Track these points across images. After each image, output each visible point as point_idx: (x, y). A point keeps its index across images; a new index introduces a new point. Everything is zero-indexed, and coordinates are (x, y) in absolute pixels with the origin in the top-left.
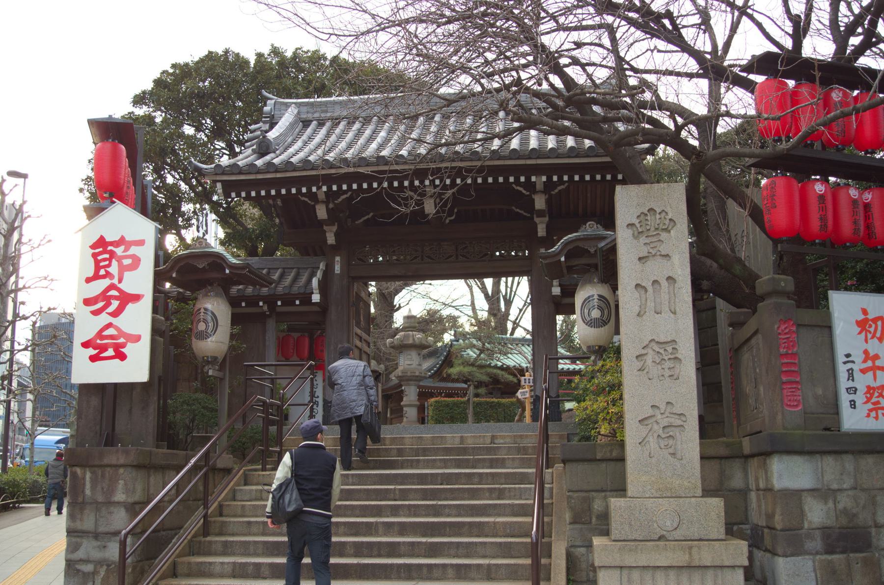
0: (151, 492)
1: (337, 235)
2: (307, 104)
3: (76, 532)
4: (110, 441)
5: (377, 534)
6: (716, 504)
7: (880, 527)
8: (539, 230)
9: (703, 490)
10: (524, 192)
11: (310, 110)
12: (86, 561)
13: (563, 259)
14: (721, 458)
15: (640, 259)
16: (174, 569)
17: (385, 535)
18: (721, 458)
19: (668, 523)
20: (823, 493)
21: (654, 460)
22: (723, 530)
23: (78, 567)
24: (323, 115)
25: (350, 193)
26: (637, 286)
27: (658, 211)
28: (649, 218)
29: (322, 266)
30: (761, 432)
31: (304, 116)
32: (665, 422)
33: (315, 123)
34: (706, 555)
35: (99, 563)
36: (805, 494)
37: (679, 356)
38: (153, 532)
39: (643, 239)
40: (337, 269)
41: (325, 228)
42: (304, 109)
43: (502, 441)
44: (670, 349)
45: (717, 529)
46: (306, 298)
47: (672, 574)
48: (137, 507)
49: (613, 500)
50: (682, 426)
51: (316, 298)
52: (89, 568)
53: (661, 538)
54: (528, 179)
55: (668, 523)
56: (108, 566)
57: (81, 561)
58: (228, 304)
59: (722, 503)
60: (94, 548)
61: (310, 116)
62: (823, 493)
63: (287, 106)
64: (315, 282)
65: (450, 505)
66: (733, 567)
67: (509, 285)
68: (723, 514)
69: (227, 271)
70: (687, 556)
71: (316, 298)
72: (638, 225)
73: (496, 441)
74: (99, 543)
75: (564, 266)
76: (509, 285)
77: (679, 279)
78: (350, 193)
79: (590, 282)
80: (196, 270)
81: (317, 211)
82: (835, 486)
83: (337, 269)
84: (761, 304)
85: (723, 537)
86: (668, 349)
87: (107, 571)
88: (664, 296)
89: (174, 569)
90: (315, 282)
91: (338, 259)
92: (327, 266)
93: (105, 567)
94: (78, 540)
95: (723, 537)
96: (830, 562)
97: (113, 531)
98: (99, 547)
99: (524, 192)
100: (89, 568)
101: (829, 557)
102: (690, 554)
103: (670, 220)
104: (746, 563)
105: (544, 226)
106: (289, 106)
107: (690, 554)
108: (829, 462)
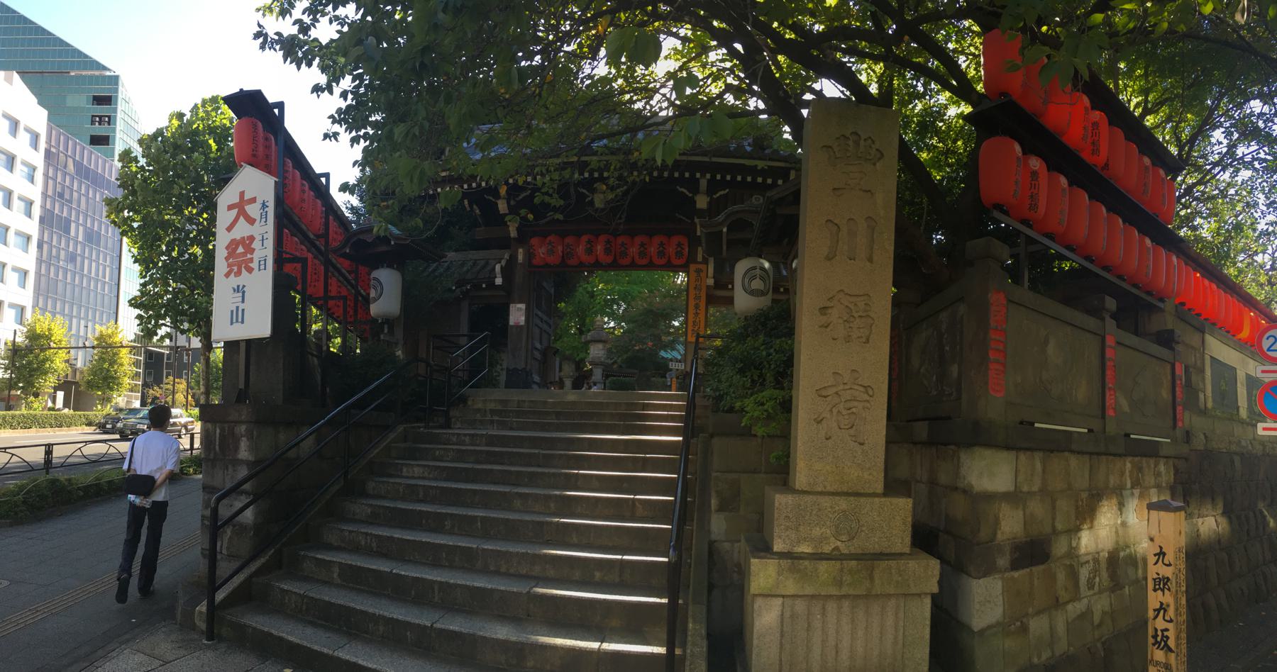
1: (518, 229)
5: (472, 505)
6: (903, 506)
14: (1091, 454)
18: (1091, 454)
20: (1015, 497)
22: (908, 540)
27: (863, 137)
30: (949, 418)
37: (872, 315)
45: (902, 541)
46: (491, 285)
49: (777, 496)
51: (499, 281)
54: (692, 175)
66: (919, 595)
71: (499, 281)
83: (520, 258)
85: (907, 550)
91: (521, 250)
95: (907, 550)
104: (935, 589)
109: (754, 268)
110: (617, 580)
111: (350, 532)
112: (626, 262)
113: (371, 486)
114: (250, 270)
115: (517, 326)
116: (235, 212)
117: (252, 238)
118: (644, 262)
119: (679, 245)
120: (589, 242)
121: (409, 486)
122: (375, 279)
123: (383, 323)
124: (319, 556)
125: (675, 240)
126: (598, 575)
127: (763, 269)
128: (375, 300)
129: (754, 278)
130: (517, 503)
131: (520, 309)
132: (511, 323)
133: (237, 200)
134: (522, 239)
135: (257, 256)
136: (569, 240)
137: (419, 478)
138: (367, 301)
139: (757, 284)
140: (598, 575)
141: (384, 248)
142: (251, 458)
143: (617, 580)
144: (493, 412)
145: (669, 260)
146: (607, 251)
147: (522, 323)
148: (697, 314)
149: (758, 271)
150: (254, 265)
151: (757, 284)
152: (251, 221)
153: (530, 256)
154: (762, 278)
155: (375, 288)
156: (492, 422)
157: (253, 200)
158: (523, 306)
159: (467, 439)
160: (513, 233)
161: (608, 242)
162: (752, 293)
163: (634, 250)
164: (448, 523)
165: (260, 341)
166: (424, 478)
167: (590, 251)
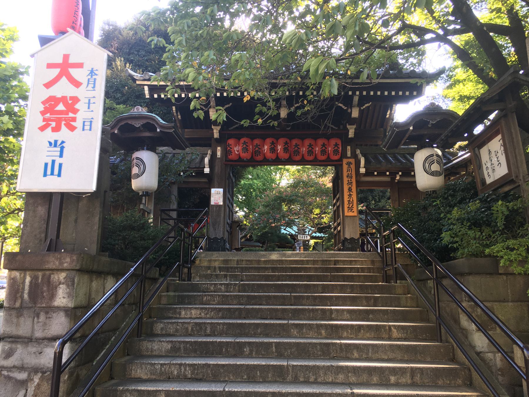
0: (93, 296)
1: (220, 132)
3: (11, 337)
4: (53, 247)
8: (350, 133)
10: (343, 107)
12: (21, 368)
13: (411, 128)
16: (111, 370)
29: (209, 152)
35: (36, 370)
38: (95, 335)
40: (219, 154)
46: (200, 172)
48: (79, 313)
51: (207, 170)
52: (23, 376)
56: (43, 373)
60: (30, 353)
64: (207, 160)
69: (158, 130)
71: (207, 170)
75: (409, 132)
80: (133, 129)
83: (219, 154)
87: (42, 379)
89: (111, 370)
90: (207, 160)
91: (219, 148)
92: (212, 152)
93: (40, 375)
94: (14, 346)
97: (50, 336)
99: (343, 107)
100: (23, 376)
109: (432, 155)
110: (409, 381)
111: (162, 365)
112: (298, 158)
113: (159, 327)
114: (72, 128)
115: (217, 206)
116: (57, 71)
117: (76, 100)
118: (311, 158)
119: (336, 145)
120: (273, 143)
121: (196, 323)
122: (137, 158)
123: (142, 196)
124: (139, 388)
125: (333, 142)
126: (393, 379)
127: (438, 155)
128: (138, 176)
129: (432, 163)
130: (295, 332)
131: (218, 193)
132: (212, 203)
133: (60, 61)
134: (221, 141)
135: (80, 117)
136: (257, 141)
137: (197, 318)
138: (129, 178)
139: (435, 167)
140: (393, 379)
141: (147, 134)
142: (71, 305)
143: (409, 381)
144: (220, 269)
145: (328, 157)
146: (286, 150)
147: (221, 203)
148: (350, 195)
149: (435, 158)
150: (78, 124)
151: (435, 167)
152: (77, 84)
153: (226, 152)
154: (438, 163)
155: (138, 165)
156: (217, 276)
157: (80, 65)
158: (221, 190)
159: (223, 288)
160: (216, 135)
161: (286, 143)
162: (433, 174)
163: (304, 150)
164: (247, 350)
165: (77, 197)
166: (201, 318)
167: (273, 149)
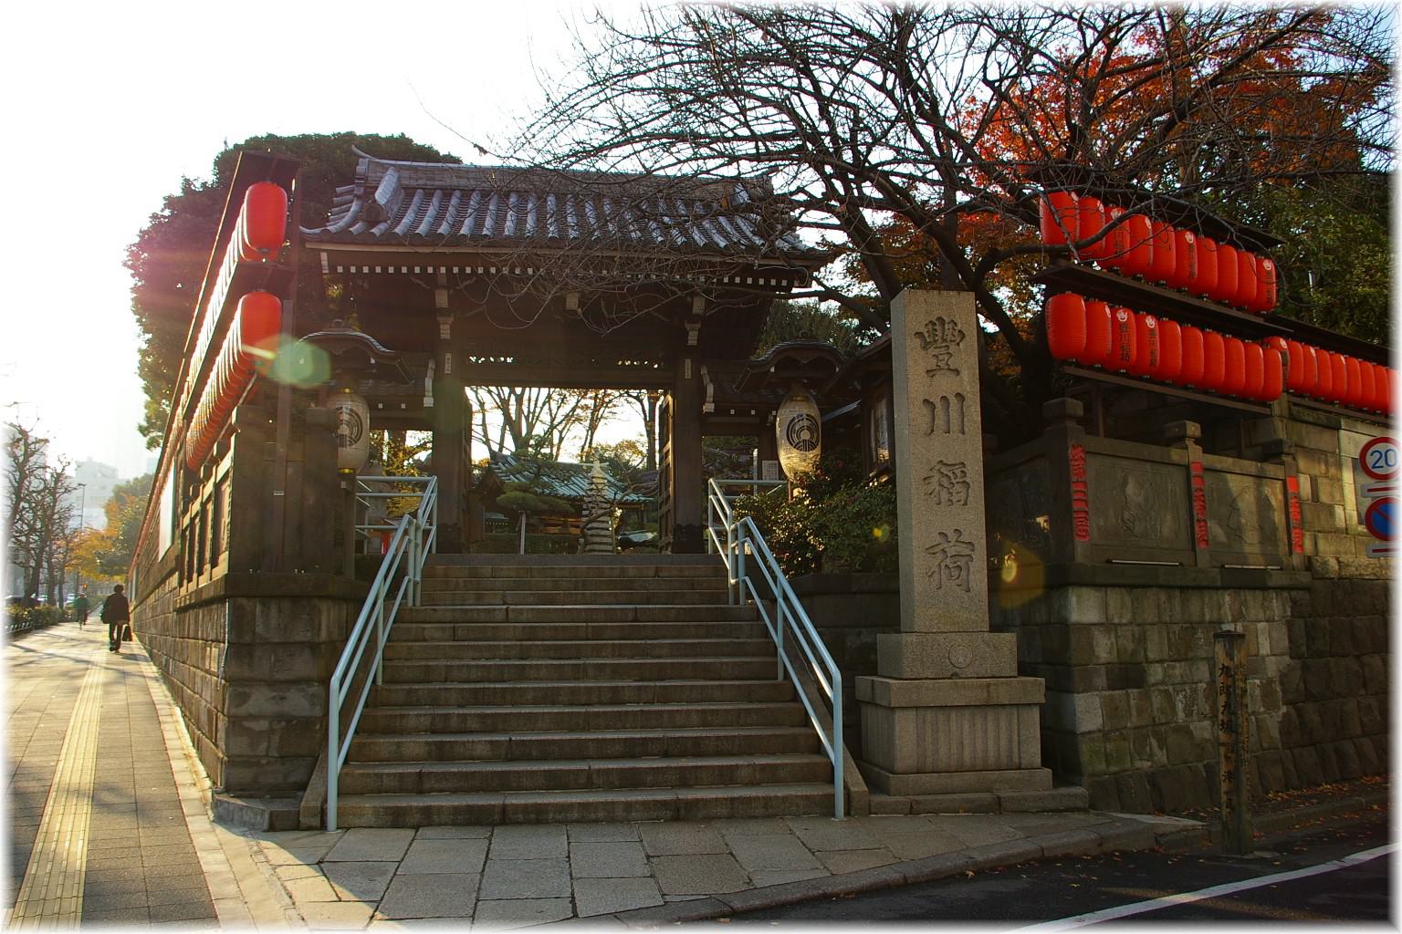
2: (409, 168)
7: (1151, 663)
9: (990, 626)
11: (413, 175)
15: (928, 371)
17: (596, 678)
19: (961, 660)
21: (941, 592)
23: (246, 724)
24: (429, 183)
25: (474, 278)
26: (926, 401)
28: (937, 327)
31: (406, 182)
32: (951, 552)
33: (457, 193)
34: (1003, 695)
36: (1093, 628)
39: (932, 351)
41: (439, 319)
42: (406, 174)
43: (667, 574)
44: (958, 472)
45: (1010, 666)
47: (967, 712)
50: (970, 555)
53: (954, 675)
55: (961, 660)
57: (251, 717)
58: (366, 406)
59: (1015, 639)
61: (413, 183)
62: (1108, 626)
63: (385, 168)
65: (686, 644)
67: (533, 399)
68: (1015, 649)
70: (985, 694)
72: (926, 335)
73: (661, 574)
74: (274, 694)
76: (533, 399)
77: (968, 396)
78: (474, 278)
79: (806, 400)
81: (437, 297)
82: (1116, 621)
84: (1048, 428)
86: (956, 471)
88: (954, 414)
91: (448, 356)
94: (247, 690)
96: (1112, 698)
98: (273, 698)
101: (1111, 692)
102: (988, 692)
103: (960, 331)
105: (696, 333)
106: (387, 169)
107: (988, 692)
108: (1114, 597)
